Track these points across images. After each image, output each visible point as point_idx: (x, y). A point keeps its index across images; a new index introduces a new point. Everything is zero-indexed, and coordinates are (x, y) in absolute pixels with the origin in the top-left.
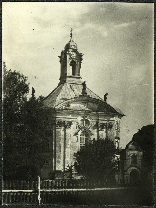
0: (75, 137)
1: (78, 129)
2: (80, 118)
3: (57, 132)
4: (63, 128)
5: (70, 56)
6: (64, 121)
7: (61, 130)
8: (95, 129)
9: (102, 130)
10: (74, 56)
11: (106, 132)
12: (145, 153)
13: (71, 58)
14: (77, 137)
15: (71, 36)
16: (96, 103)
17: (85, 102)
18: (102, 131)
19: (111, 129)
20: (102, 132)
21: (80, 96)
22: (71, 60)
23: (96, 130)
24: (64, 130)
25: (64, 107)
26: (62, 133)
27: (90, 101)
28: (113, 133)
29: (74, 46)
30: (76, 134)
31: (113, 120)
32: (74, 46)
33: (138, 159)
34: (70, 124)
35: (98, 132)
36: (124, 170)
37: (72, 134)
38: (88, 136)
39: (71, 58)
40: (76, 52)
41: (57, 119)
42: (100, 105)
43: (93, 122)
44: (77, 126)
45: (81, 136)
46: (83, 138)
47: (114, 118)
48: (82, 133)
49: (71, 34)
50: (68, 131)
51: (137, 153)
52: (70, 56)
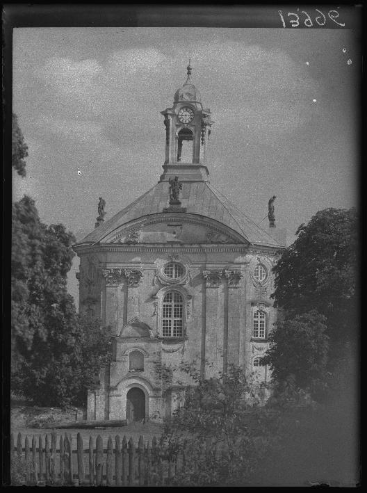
0: (150, 306)
1: (157, 286)
2: (160, 264)
3: (108, 295)
4: (121, 286)
5: (178, 120)
6: (123, 270)
7: (116, 290)
8: (197, 285)
9: (215, 285)
10: (188, 117)
11: (226, 290)
12: (37, 354)
13: (180, 124)
14: (155, 305)
15: (189, 73)
16: (199, 224)
17: (174, 223)
18: (215, 288)
19: (237, 283)
20: (214, 290)
21: (166, 211)
22: (179, 129)
23: (200, 287)
24: (125, 290)
25: (123, 240)
26: (120, 295)
27: (185, 221)
28: (243, 293)
29: (189, 94)
30: (153, 297)
31: (244, 261)
32: (189, 94)
33: (146, 360)
34: (137, 275)
35: (204, 291)
36: (111, 385)
37: (143, 298)
38: (181, 301)
39: (180, 124)
40: (190, 108)
41: (109, 266)
42: (211, 228)
43: (192, 270)
44: (154, 280)
45: (164, 301)
46: (170, 306)
47: (247, 256)
48: (167, 298)
49: (189, 69)
50: (134, 292)
51: (144, 348)
52: (178, 120)
